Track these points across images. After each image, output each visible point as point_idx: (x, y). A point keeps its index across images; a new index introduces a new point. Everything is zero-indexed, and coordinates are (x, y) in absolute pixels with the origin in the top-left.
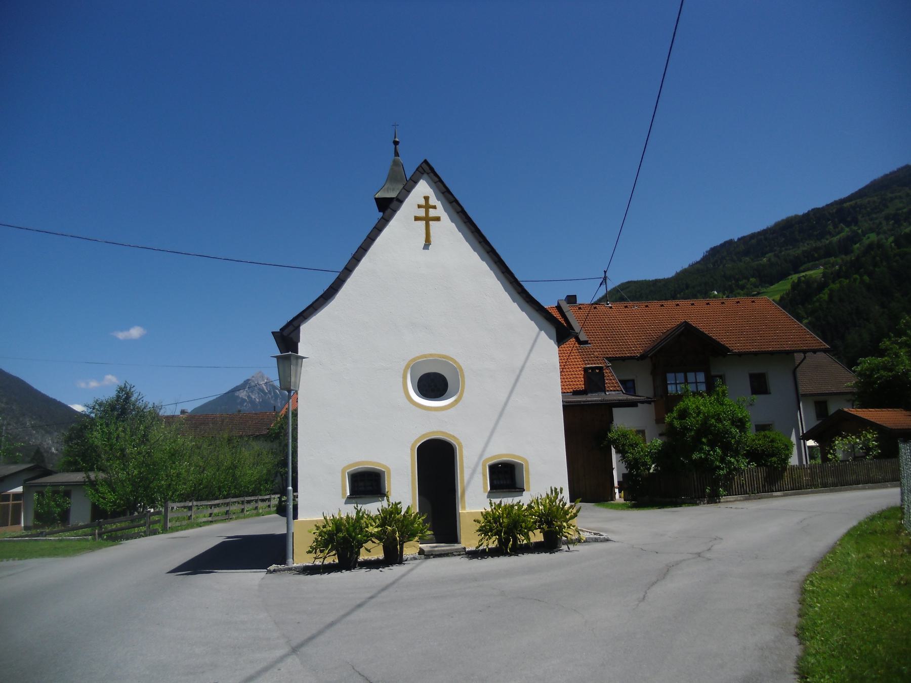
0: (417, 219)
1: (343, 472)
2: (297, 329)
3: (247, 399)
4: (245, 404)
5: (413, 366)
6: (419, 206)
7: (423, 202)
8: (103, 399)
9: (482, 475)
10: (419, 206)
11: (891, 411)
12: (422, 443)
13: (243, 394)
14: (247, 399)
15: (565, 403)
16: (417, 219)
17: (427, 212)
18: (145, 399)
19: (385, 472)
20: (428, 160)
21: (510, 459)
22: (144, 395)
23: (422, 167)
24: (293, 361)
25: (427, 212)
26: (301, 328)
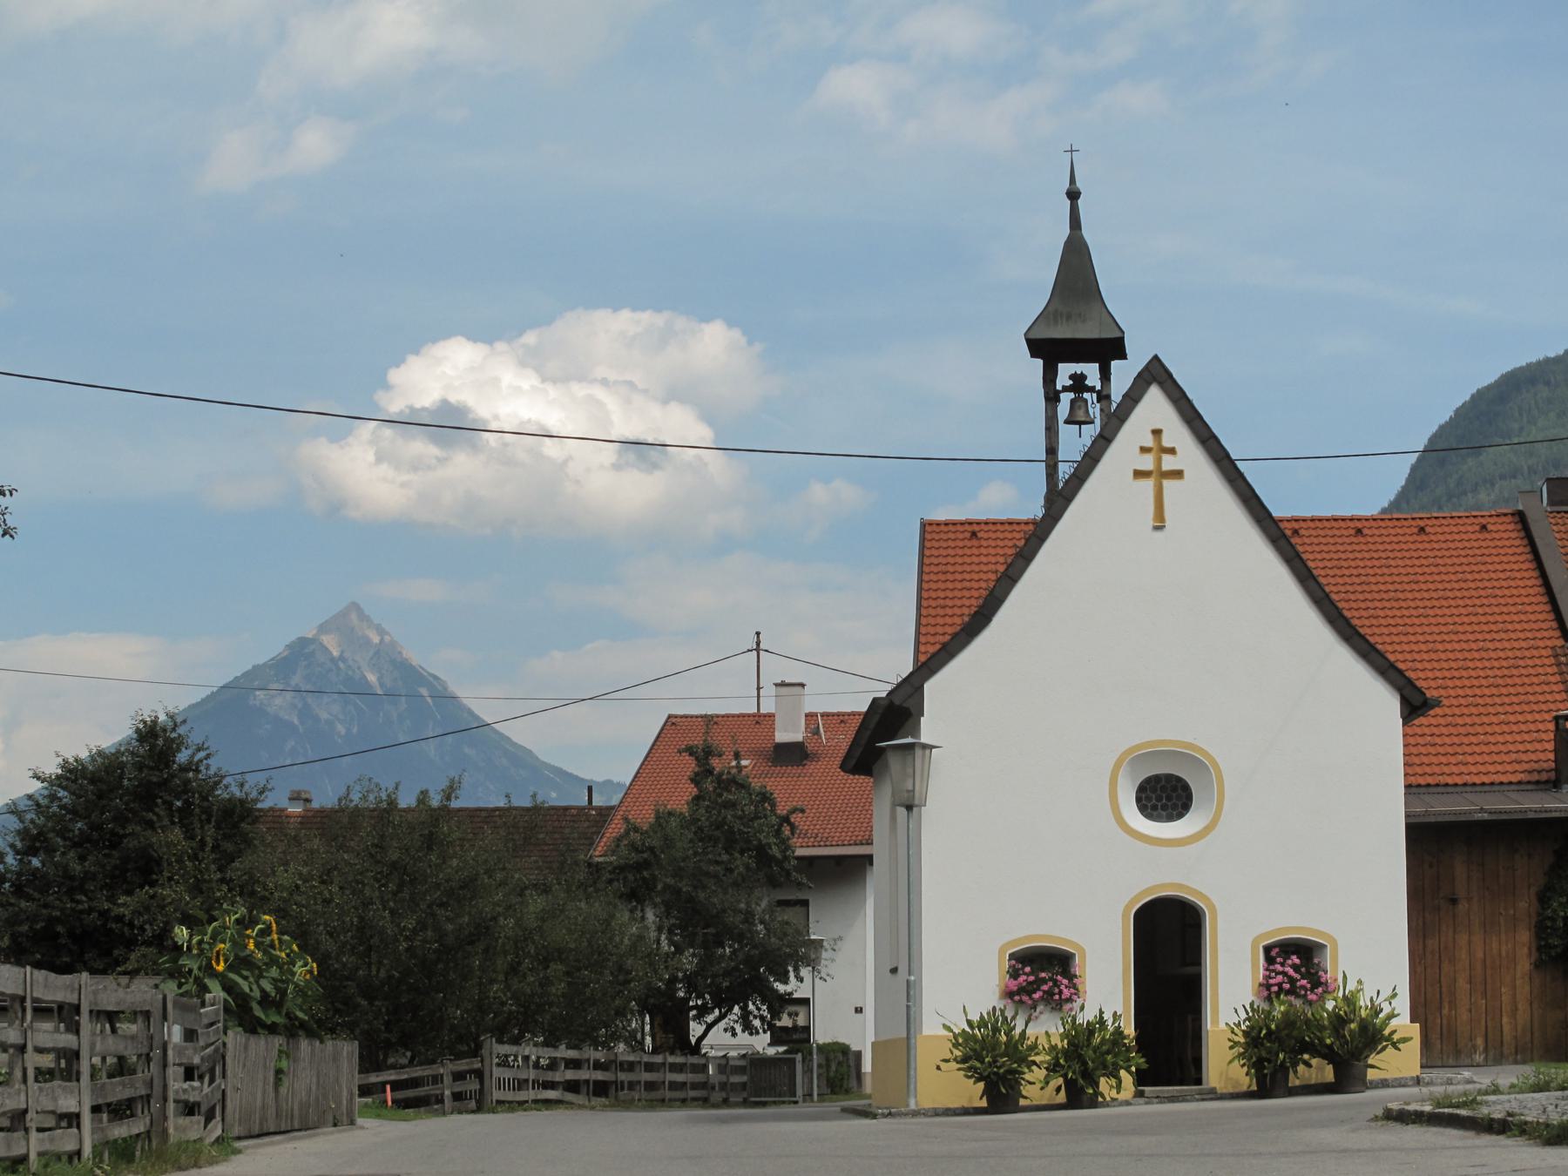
0: (1139, 474)
1: (1002, 951)
2: (919, 691)
3: (296, 721)
4: (290, 744)
5: (1138, 757)
6: (1144, 450)
7: (1149, 441)
8: (84, 755)
9: (130, 1096)
10: (1144, 450)
11: (915, 1028)
12: (1146, 903)
13: (280, 704)
14: (296, 721)
15: (1412, 820)
16: (1139, 474)
17: (1159, 461)
18: (214, 764)
19: (1075, 954)
20: (1159, 356)
21: (1276, 939)
22: (212, 750)
23: (1149, 371)
24: (918, 752)
25: (1159, 461)
26: (926, 686)
